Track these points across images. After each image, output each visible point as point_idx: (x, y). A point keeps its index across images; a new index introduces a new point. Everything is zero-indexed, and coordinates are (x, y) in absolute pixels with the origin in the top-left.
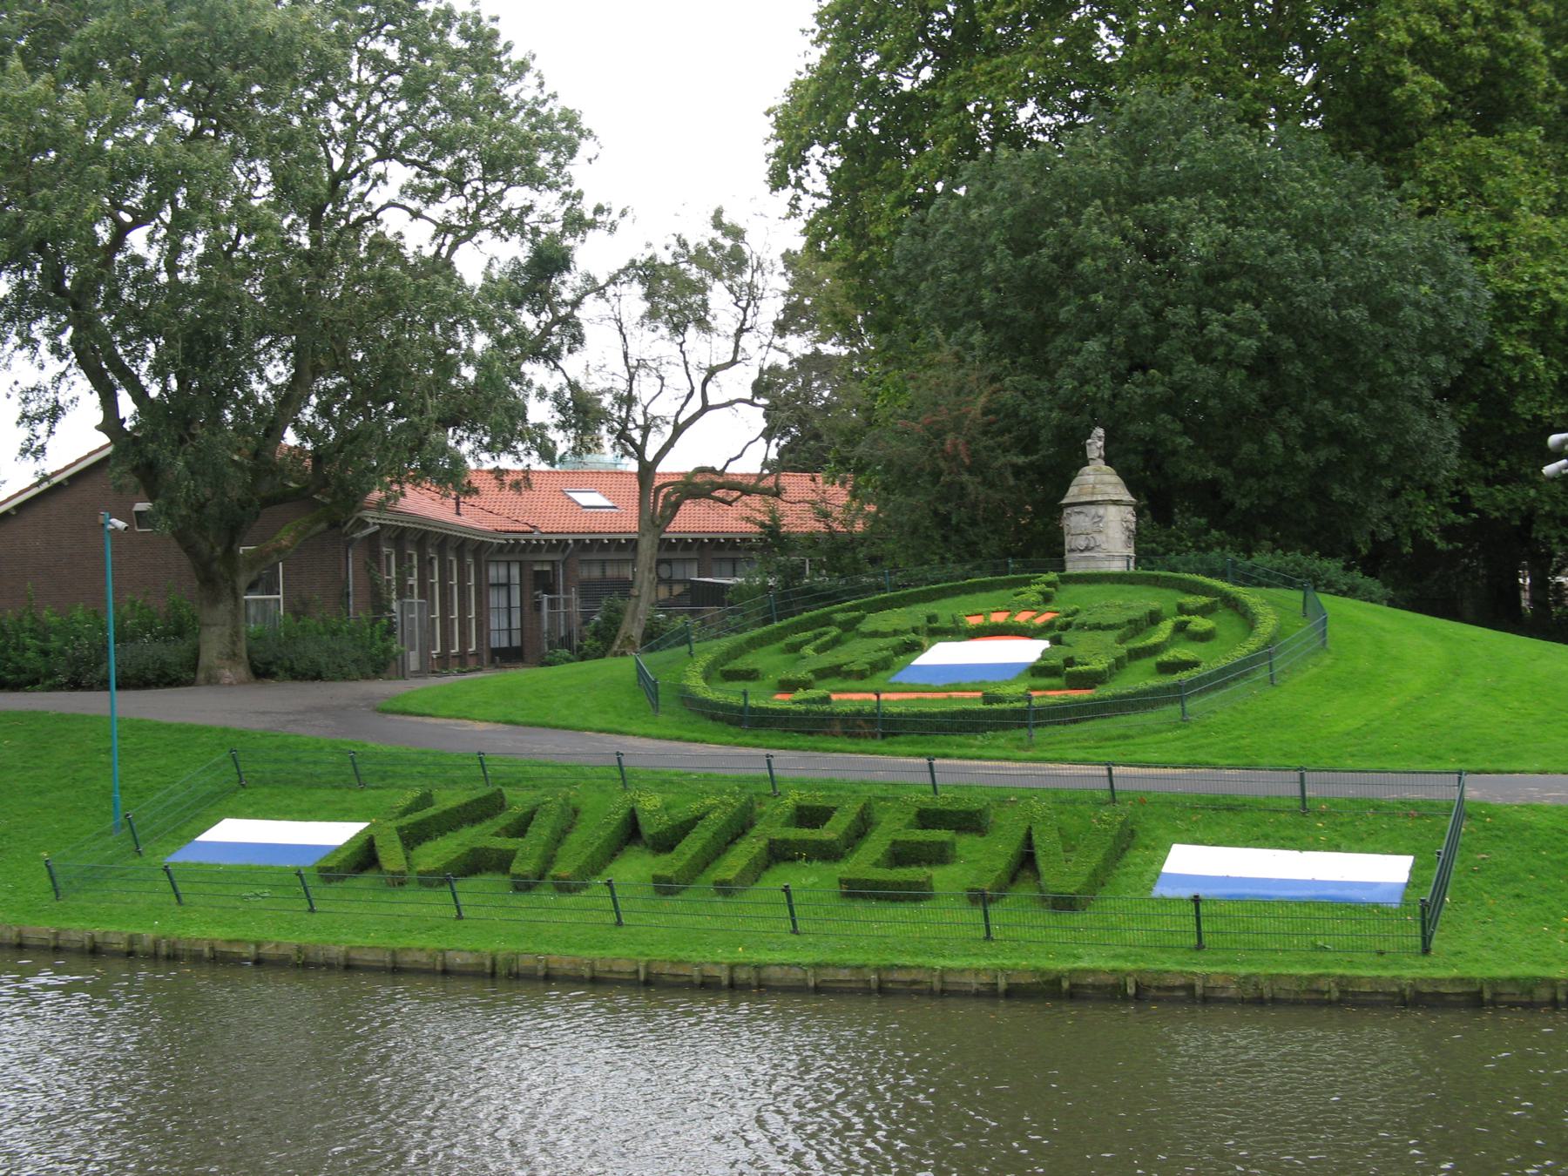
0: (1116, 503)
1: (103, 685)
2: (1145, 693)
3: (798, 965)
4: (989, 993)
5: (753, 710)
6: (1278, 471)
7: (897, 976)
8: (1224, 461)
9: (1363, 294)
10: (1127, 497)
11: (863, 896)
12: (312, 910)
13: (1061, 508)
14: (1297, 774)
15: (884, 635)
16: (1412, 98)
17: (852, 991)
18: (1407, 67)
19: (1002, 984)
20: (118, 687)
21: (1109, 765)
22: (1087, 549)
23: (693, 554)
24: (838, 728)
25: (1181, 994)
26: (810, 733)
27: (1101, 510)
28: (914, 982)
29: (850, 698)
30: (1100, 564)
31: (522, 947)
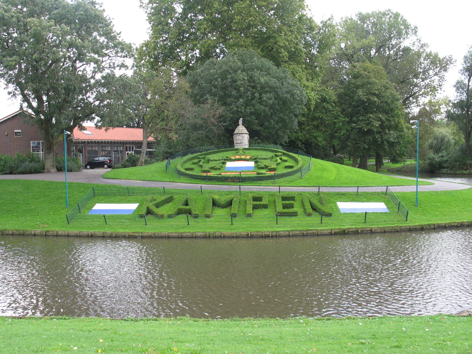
0: (246, 134)
1: (78, 169)
3: (287, 231)
4: (331, 234)
5: (208, 177)
6: (272, 128)
7: (309, 232)
9: (287, 92)
10: (247, 132)
11: (283, 216)
12: (146, 224)
15: (216, 161)
18: (283, 51)
19: (333, 232)
20: (68, 171)
21: (279, 186)
23: (110, 145)
24: (230, 180)
26: (224, 182)
27: (244, 135)
29: (213, 174)
31: (216, 230)
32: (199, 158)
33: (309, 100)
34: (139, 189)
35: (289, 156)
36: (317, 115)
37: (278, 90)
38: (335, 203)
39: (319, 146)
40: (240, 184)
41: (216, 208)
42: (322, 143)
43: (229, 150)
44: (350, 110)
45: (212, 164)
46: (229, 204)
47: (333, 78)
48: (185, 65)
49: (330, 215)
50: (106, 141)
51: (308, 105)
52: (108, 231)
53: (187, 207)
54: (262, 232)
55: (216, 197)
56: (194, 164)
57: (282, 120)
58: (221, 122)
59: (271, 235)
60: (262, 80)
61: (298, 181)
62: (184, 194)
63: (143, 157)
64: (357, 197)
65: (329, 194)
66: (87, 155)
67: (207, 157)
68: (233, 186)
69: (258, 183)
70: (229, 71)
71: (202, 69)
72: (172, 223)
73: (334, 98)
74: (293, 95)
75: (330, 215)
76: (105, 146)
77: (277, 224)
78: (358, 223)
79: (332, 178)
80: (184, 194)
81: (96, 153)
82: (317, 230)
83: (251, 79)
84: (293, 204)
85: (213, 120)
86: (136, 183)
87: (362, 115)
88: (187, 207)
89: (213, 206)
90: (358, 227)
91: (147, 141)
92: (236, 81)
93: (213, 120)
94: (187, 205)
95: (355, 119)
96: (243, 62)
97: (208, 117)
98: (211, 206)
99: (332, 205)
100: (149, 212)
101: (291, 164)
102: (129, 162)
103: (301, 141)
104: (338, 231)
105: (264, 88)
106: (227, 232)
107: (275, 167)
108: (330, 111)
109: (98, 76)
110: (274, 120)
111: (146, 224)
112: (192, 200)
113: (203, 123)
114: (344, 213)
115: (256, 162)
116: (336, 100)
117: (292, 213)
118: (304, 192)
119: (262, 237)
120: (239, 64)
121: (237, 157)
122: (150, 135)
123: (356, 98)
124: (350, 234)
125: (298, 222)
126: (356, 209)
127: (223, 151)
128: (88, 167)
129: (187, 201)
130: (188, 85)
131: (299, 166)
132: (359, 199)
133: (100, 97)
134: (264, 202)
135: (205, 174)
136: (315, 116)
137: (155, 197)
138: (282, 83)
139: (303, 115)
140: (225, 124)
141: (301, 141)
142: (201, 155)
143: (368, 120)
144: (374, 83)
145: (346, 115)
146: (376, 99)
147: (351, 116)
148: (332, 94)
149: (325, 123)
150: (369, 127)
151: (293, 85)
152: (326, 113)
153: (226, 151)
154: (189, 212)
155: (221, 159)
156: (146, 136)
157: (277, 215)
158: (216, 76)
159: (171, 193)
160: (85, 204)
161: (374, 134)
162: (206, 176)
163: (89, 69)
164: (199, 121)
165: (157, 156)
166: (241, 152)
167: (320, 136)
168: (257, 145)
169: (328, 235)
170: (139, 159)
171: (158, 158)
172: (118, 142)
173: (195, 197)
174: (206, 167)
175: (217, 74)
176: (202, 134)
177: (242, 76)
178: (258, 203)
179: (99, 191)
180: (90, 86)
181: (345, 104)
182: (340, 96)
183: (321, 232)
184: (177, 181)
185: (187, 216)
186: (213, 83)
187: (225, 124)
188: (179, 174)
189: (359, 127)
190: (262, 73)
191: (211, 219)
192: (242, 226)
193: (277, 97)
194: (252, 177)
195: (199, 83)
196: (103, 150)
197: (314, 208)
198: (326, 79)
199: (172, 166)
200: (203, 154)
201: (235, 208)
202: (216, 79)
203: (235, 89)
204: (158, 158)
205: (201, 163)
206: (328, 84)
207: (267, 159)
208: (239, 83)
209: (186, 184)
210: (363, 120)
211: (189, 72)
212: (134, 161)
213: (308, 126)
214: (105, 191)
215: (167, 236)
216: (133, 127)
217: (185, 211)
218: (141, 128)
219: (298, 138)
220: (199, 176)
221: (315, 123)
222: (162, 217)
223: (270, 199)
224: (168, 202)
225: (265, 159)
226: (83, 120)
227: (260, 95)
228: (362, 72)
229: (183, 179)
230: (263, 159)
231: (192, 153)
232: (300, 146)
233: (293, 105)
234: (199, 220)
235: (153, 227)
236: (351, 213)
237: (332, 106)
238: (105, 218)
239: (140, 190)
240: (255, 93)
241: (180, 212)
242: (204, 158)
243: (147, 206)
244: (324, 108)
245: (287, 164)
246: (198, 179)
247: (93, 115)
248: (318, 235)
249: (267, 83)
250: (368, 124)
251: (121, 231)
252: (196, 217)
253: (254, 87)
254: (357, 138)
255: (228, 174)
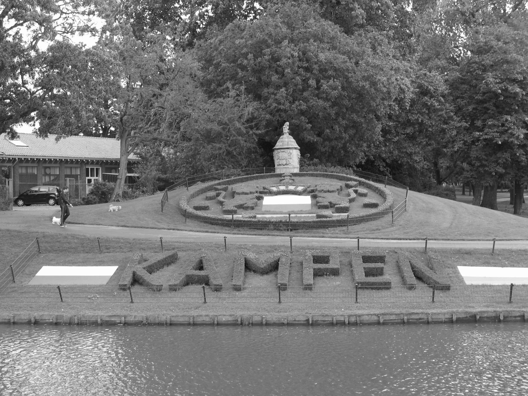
0: (296, 148)
2: (370, 215)
3: (375, 315)
4: (450, 322)
5: (235, 221)
7: (413, 317)
8: (319, 135)
9: (365, 78)
10: (297, 146)
11: (367, 288)
12: (132, 302)
13: (273, 150)
14: (425, 241)
16: (357, 16)
17: (397, 323)
19: (454, 318)
22: (286, 164)
23: (58, 165)
24: (272, 227)
25: (519, 318)
26: (261, 229)
27: (291, 151)
28: (420, 319)
30: (291, 170)
31: (253, 313)
32: (216, 189)
33: (402, 91)
34: (118, 241)
35: (369, 187)
36: (413, 118)
37: (350, 75)
38: (455, 268)
39: (415, 169)
40: (289, 233)
41: (251, 275)
42: (421, 164)
43: (267, 177)
44: (470, 108)
45: (239, 200)
46: (274, 267)
47: (439, 55)
48: (189, 29)
49: (447, 288)
50: (52, 159)
51: (400, 102)
52: (66, 313)
53: (202, 273)
54: (332, 316)
55: (251, 256)
56: (208, 199)
57: (355, 125)
58: (251, 128)
59: (347, 322)
60: (322, 57)
61: (387, 230)
62: (195, 250)
63: (120, 187)
64: (492, 258)
65: (444, 252)
66: (18, 182)
67: (230, 187)
68: (277, 238)
69: (318, 233)
70: (267, 41)
71: (220, 37)
72: (176, 300)
73: (443, 88)
74: (374, 84)
75: (447, 288)
76: (49, 168)
77: (357, 302)
78: (498, 303)
79: (446, 225)
80: (195, 250)
81: (34, 180)
82: (427, 314)
83: (304, 56)
84: (382, 269)
85: (238, 125)
86: (111, 232)
87: (492, 117)
88: (202, 273)
89: (246, 271)
90: (498, 309)
91: (127, 158)
92: (278, 60)
93: (238, 125)
94: (201, 268)
95: (479, 123)
96: (290, 26)
97: (231, 120)
98: (243, 271)
99: (450, 271)
100: (136, 280)
101: (374, 201)
102: (96, 195)
103: (384, 160)
104: (463, 316)
105: (326, 70)
106: (272, 316)
107: (347, 205)
108: (436, 110)
109: (43, 46)
110: (340, 126)
111: (132, 302)
112: (209, 261)
113: (222, 131)
114: (472, 286)
115: (314, 197)
116: (446, 92)
117: (381, 284)
118: (401, 249)
119: (332, 324)
120: (284, 29)
121: (282, 188)
122: (132, 151)
123: (482, 86)
124: (484, 322)
125: (393, 300)
126: (491, 279)
127: (257, 178)
128: (21, 202)
129: (201, 262)
130: (196, 65)
131: (388, 204)
132: (497, 261)
133: (45, 84)
134: (332, 265)
135: (229, 217)
136: (411, 121)
137: (146, 254)
138: (357, 63)
139: (390, 117)
140: (260, 132)
141: (384, 160)
142: (219, 184)
143: (503, 125)
144: (516, 62)
145: (463, 118)
146: (518, 90)
147: (473, 118)
148: (438, 81)
149: (427, 130)
150: (505, 137)
151: (375, 67)
152: (428, 114)
153: (262, 177)
154: (205, 281)
155: (254, 191)
156: (125, 152)
157: (357, 288)
158: (245, 50)
159: (174, 249)
160: (24, 266)
161: (512, 149)
162: (231, 221)
163: (27, 33)
164: (216, 127)
165: (144, 185)
166: (287, 179)
167: (419, 153)
168: (313, 168)
169: (445, 322)
170: (113, 189)
171: (145, 189)
172: (72, 161)
173: (215, 255)
174: (230, 204)
175: (246, 46)
176: (220, 149)
177: (288, 50)
178: (323, 266)
179: (46, 245)
180: (29, 62)
181: (463, 98)
182: (453, 85)
183: (434, 317)
184: (182, 228)
185: (204, 288)
186: (239, 62)
187: (260, 132)
188: (184, 215)
189: (486, 137)
190: (322, 45)
191: (244, 293)
192: (297, 306)
193: (347, 85)
194: (310, 222)
195: (215, 62)
196: (46, 174)
197: (419, 277)
198: (426, 55)
199: (171, 202)
200: (224, 183)
201: (283, 275)
202: (245, 56)
203: (277, 72)
204: (145, 189)
205: (220, 198)
206: (430, 64)
207: (333, 191)
208: (284, 61)
209: (197, 233)
210: (494, 125)
211: (197, 43)
212: (103, 193)
213: (397, 135)
214: (58, 243)
215: (168, 322)
216: (97, 135)
217: (199, 278)
218: (113, 135)
219: (380, 156)
220: (218, 220)
221: (409, 130)
222: (159, 289)
223: (342, 259)
224: (168, 264)
225: (329, 191)
226: (17, 121)
227: (318, 82)
228: (494, 43)
229: (191, 223)
230: (325, 192)
231: (203, 181)
232: (382, 169)
233: (374, 101)
234: (223, 294)
235: (143, 306)
236: (483, 286)
237: (439, 101)
238: (59, 291)
239: (118, 242)
240: (308, 79)
241: (189, 281)
242: (225, 190)
243: (133, 270)
244: (425, 105)
245: (367, 200)
246: (217, 224)
247: (33, 114)
248: (428, 323)
249: (331, 63)
250: (502, 133)
251: (88, 313)
252: (218, 289)
253: (307, 69)
254: (484, 157)
255: (268, 216)
